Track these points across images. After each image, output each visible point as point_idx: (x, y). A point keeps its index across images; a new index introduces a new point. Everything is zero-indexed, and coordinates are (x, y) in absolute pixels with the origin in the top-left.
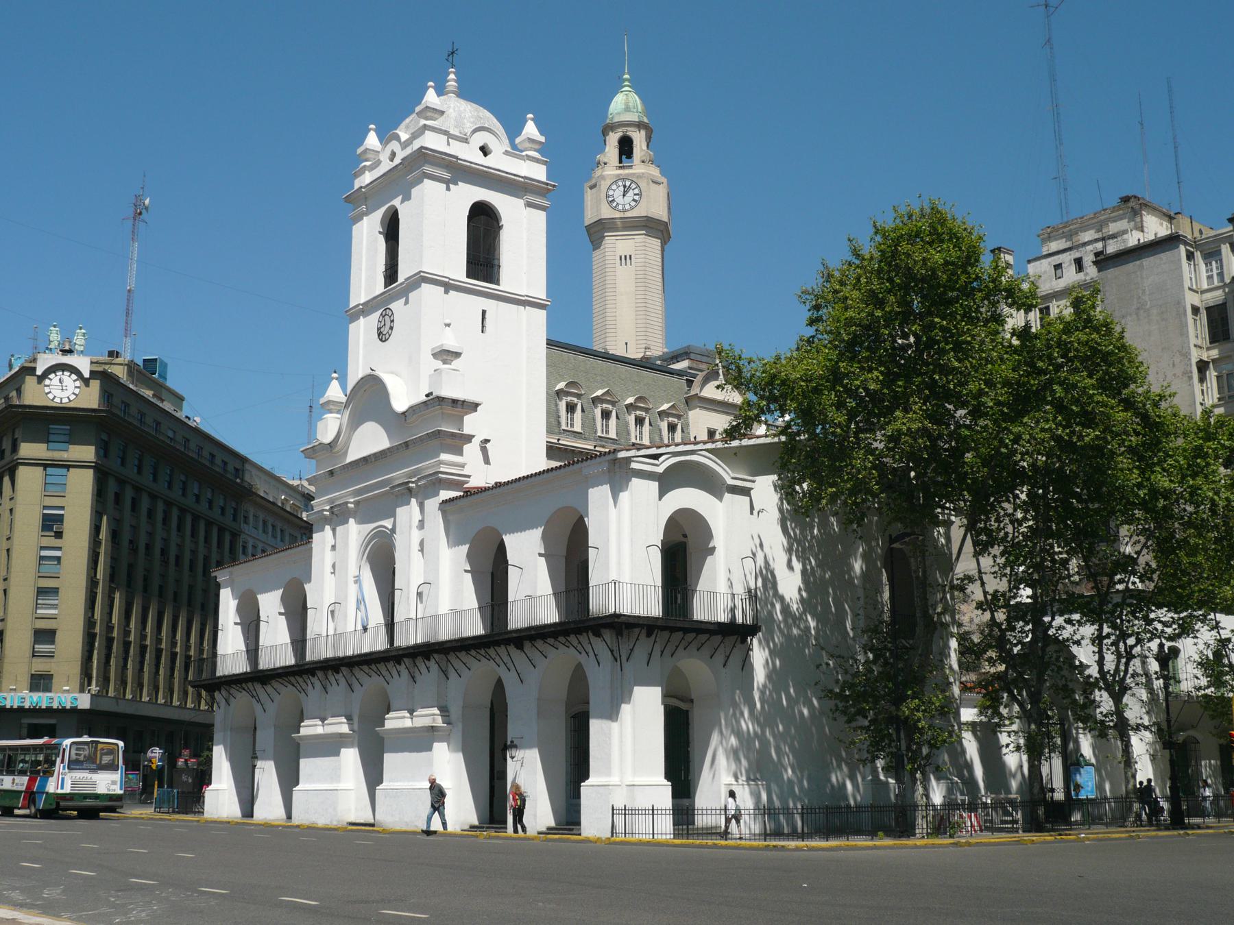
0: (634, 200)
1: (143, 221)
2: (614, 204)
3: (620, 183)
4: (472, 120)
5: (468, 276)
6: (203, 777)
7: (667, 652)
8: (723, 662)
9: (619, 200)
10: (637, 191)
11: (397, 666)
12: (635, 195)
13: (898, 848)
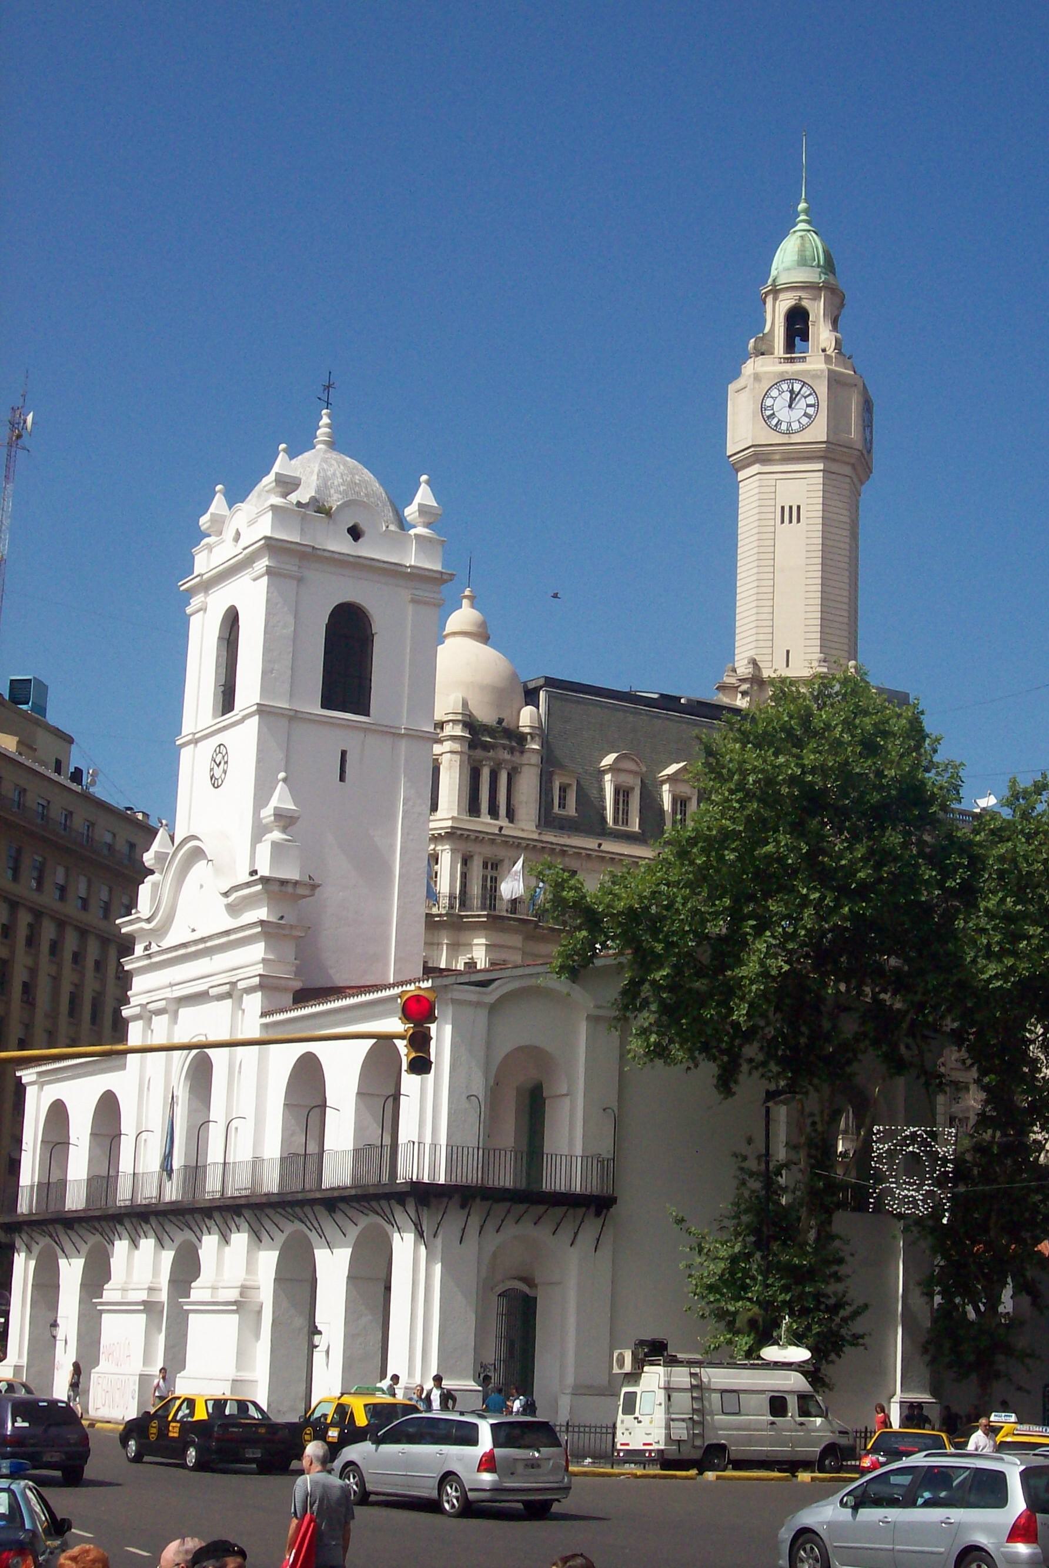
0: (806, 415)
1: (24, 448)
2: (774, 422)
3: (785, 387)
4: (342, 488)
5: (323, 707)
6: (763, 1322)
7: (490, 1227)
8: (571, 1242)
9: (783, 414)
10: (811, 400)
11: (236, 1219)
12: (808, 406)
13: (772, 1479)
